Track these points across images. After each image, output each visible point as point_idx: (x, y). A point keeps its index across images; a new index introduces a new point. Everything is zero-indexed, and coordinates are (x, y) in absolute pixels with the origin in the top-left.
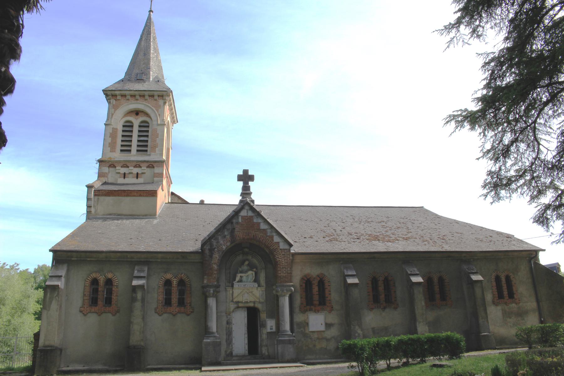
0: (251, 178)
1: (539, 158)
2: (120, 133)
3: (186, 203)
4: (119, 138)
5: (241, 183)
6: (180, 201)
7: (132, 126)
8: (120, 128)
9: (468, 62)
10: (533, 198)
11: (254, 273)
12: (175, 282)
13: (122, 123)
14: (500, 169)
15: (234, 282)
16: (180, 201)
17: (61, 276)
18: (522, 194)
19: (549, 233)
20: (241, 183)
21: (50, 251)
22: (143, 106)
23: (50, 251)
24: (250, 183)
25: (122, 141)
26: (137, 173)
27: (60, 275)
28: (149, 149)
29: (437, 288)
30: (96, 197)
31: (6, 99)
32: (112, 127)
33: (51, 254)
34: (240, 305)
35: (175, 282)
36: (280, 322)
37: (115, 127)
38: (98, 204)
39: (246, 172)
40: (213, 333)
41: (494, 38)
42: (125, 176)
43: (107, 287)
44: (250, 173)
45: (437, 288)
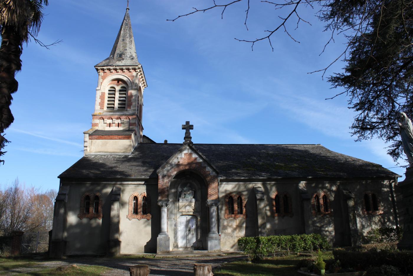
0: (191, 127)
1: (394, 111)
2: (107, 95)
3: (155, 143)
4: (106, 99)
5: (185, 131)
6: (153, 143)
7: (115, 91)
8: (107, 92)
9: (336, 45)
10: (389, 138)
11: (193, 192)
12: (140, 198)
13: (108, 88)
14: (365, 118)
15: (180, 198)
16: (153, 143)
17: (65, 194)
18: (381, 136)
19: (396, 163)
20: (185, 131)
21: (58, 177)
22: (122, 76)
23: (58, 177)
24: (191, 131)
25: (108, 101)
26: (119, 123)
27: (65, 193)
28: (126, 106)
29: (371, 202)
30: (91, 140)
31: (13, 95)
32: (101, 91)
33: (59, 179)
34: (184, 214)
35: (140, 198)
36: (210, 225)
37: (103, 92)
38: (91, 145)
39: (188, 123)
40: (164, 232)
41: (362, 25)
42: (110, 125)
43: (96, 201)
44: (190, 124)
45: (371, 202)
